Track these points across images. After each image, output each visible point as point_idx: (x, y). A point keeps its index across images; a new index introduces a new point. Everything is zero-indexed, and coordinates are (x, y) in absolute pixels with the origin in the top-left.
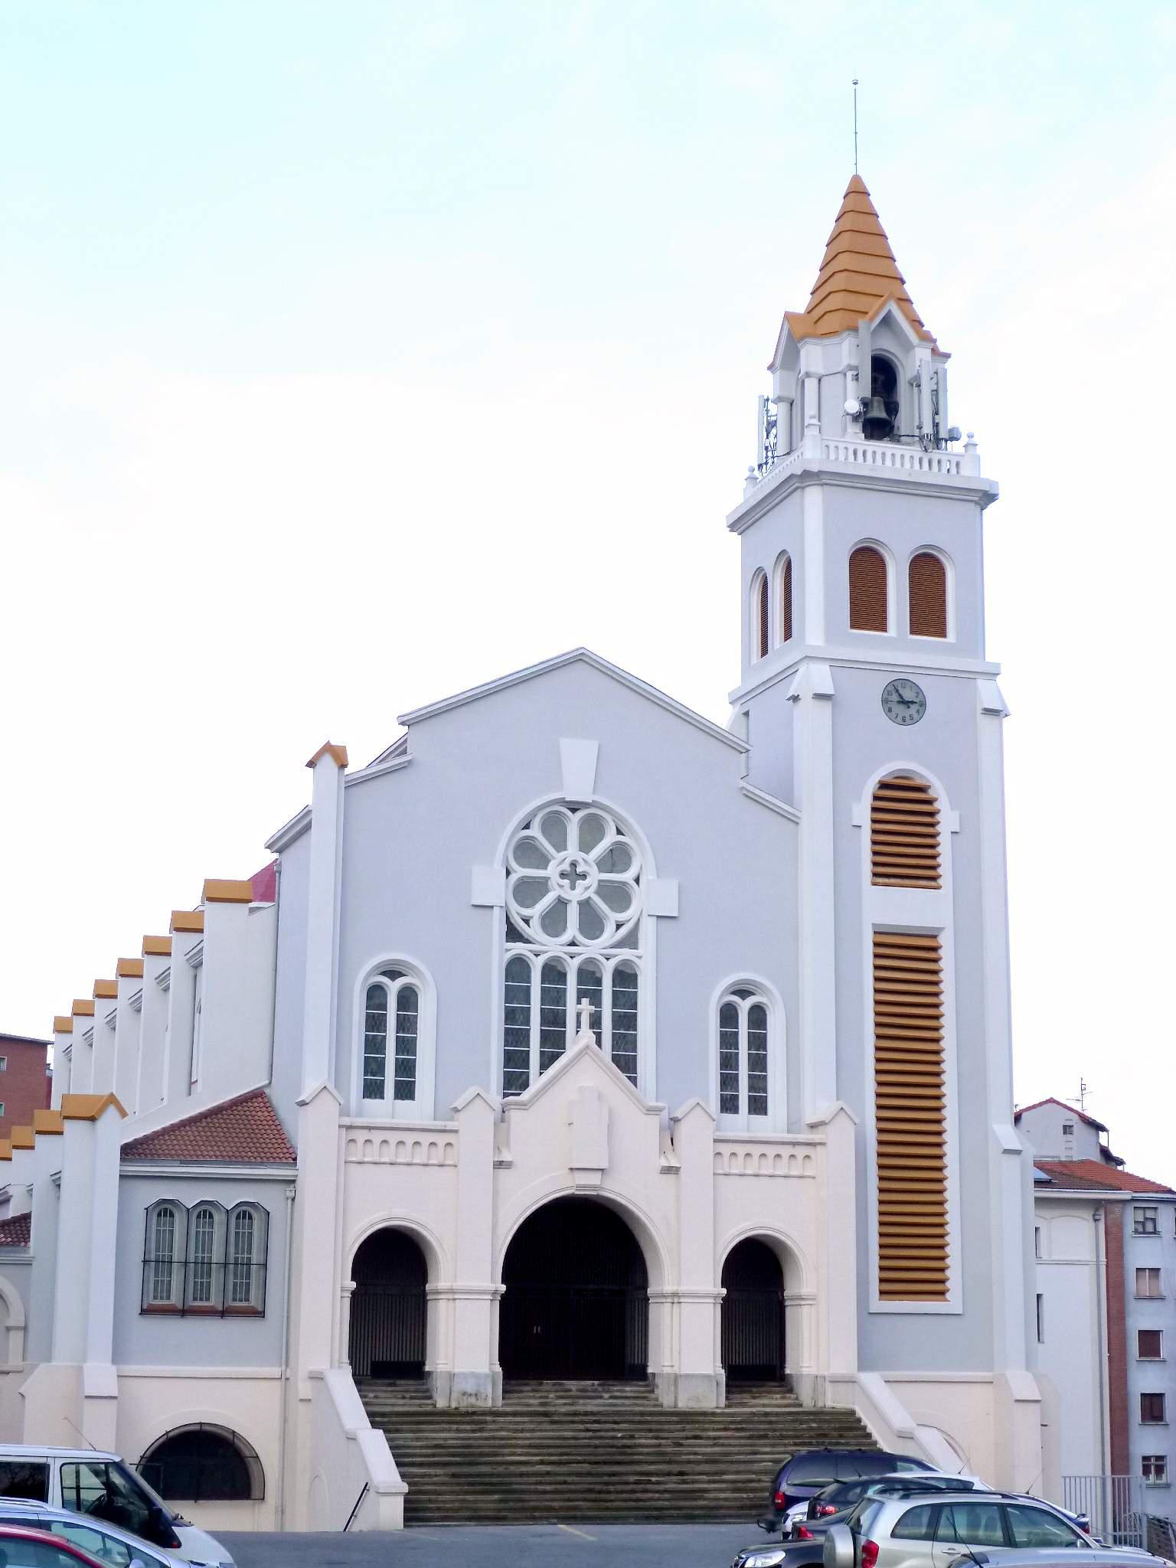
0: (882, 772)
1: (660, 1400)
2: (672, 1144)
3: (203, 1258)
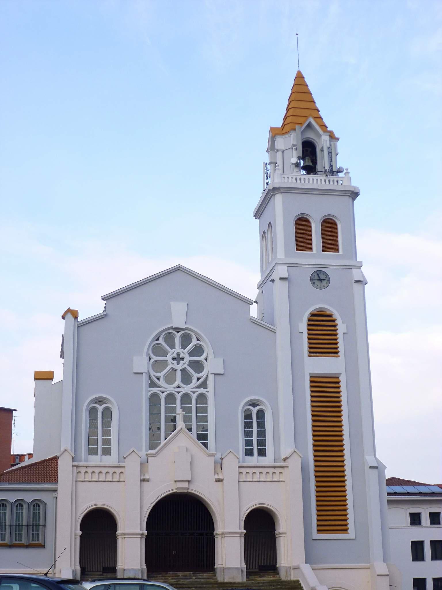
0: (312, 309)
1: (218, 579)
2: (221, 470)
3: (19, 523)
